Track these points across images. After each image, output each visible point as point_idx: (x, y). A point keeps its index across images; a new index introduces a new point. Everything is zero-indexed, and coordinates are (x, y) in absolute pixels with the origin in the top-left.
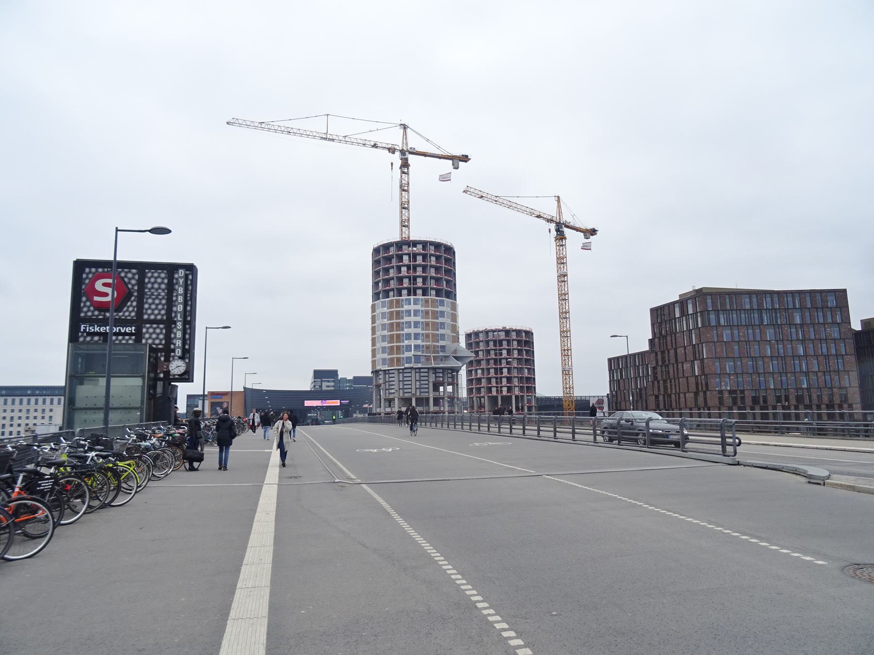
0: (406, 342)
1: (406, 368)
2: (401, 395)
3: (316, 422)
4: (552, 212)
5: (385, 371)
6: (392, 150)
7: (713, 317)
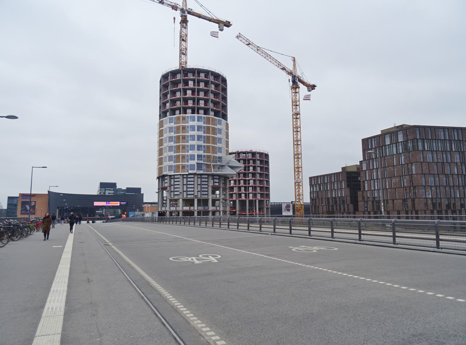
0: (191, 152)
1: (189, 174)
2: (185, 196)
3: (103, 218)
4: (290, 67)
5: (171, 176)
6: (175, 8)
7: (420, 144)
